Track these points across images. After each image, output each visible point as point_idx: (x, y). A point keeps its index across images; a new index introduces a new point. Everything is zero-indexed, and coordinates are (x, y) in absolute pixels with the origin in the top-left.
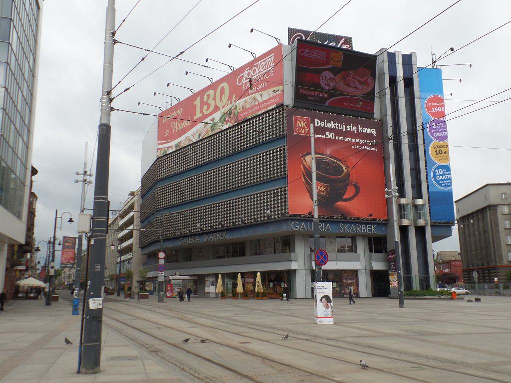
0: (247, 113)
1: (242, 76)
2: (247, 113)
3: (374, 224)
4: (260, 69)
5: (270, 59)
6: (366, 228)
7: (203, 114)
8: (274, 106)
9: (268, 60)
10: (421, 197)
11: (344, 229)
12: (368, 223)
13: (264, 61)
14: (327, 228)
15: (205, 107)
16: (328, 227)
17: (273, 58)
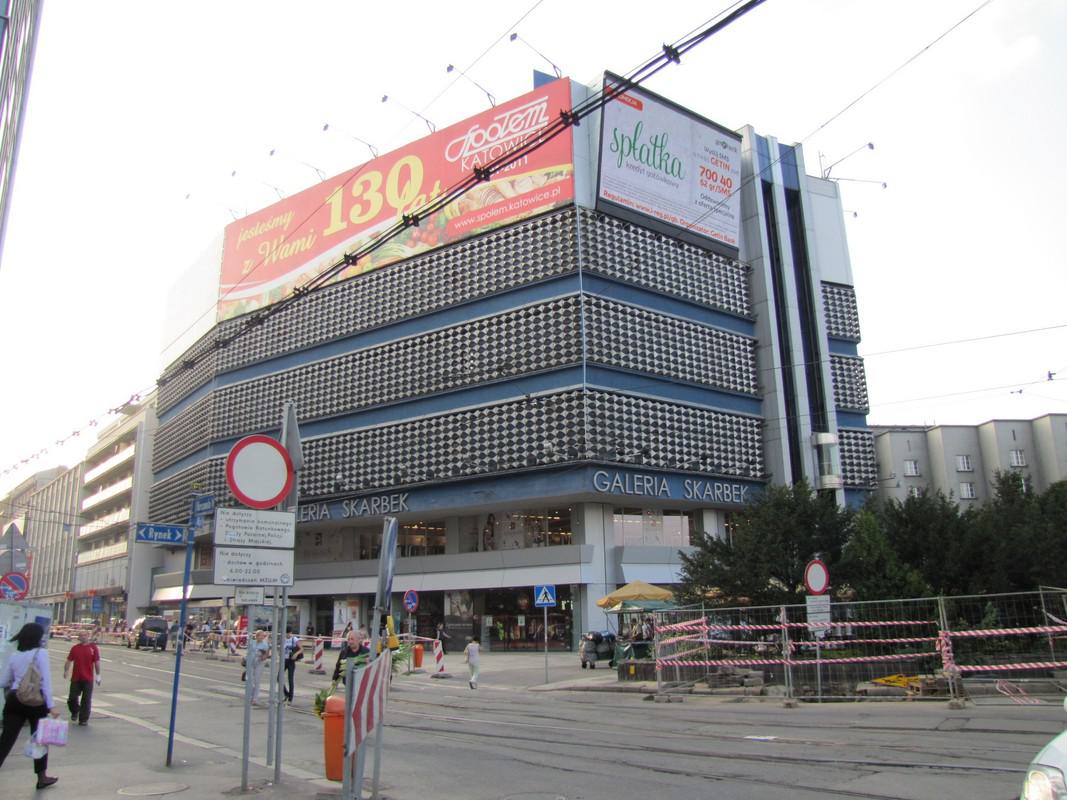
0: (472, 221)
1: (462, 142)
2: (472, 221)
4: (511, 129)
5: (538, 108)
7: (349, 222)
8: (550, 207)
9: (531, 111)
10: (825, 429)
13: (522, 112)
15: (357, 209)
16: (617, 482)
17: (545, 105)
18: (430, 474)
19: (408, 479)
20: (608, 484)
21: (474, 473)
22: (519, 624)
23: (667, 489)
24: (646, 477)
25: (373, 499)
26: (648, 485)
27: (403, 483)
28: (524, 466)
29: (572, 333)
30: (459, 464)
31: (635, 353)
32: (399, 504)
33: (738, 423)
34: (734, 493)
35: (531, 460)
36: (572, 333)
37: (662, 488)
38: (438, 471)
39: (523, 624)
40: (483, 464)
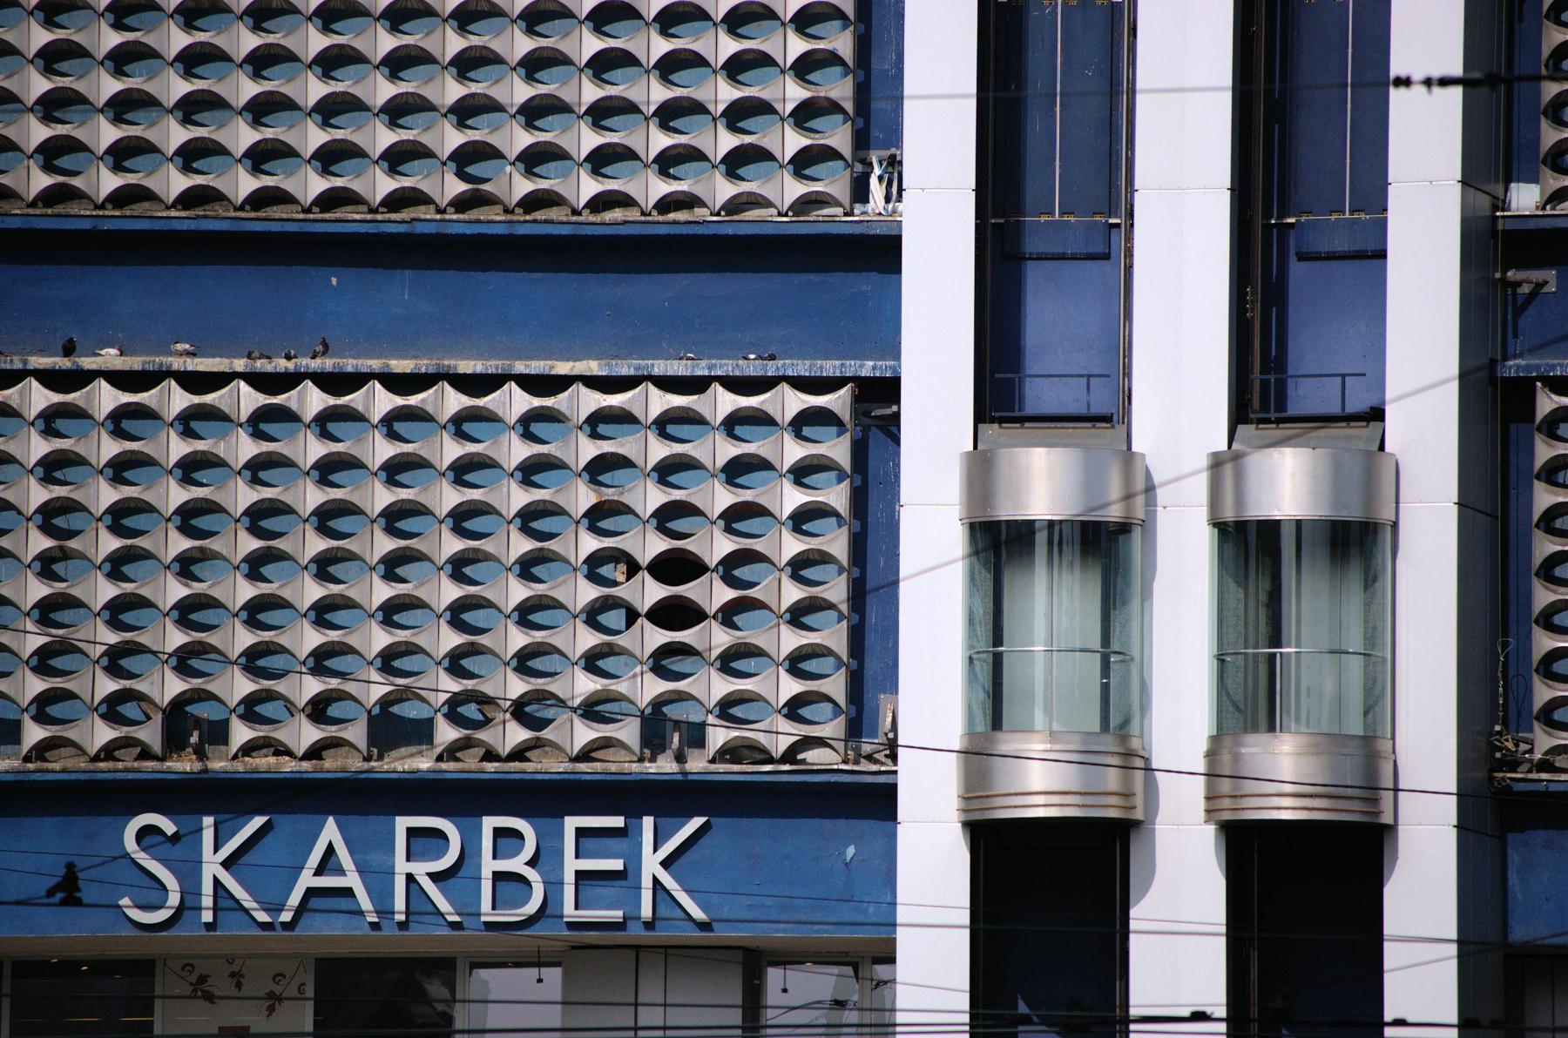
11: (189, 873)
16: (328, 863)
34: (572, 865)
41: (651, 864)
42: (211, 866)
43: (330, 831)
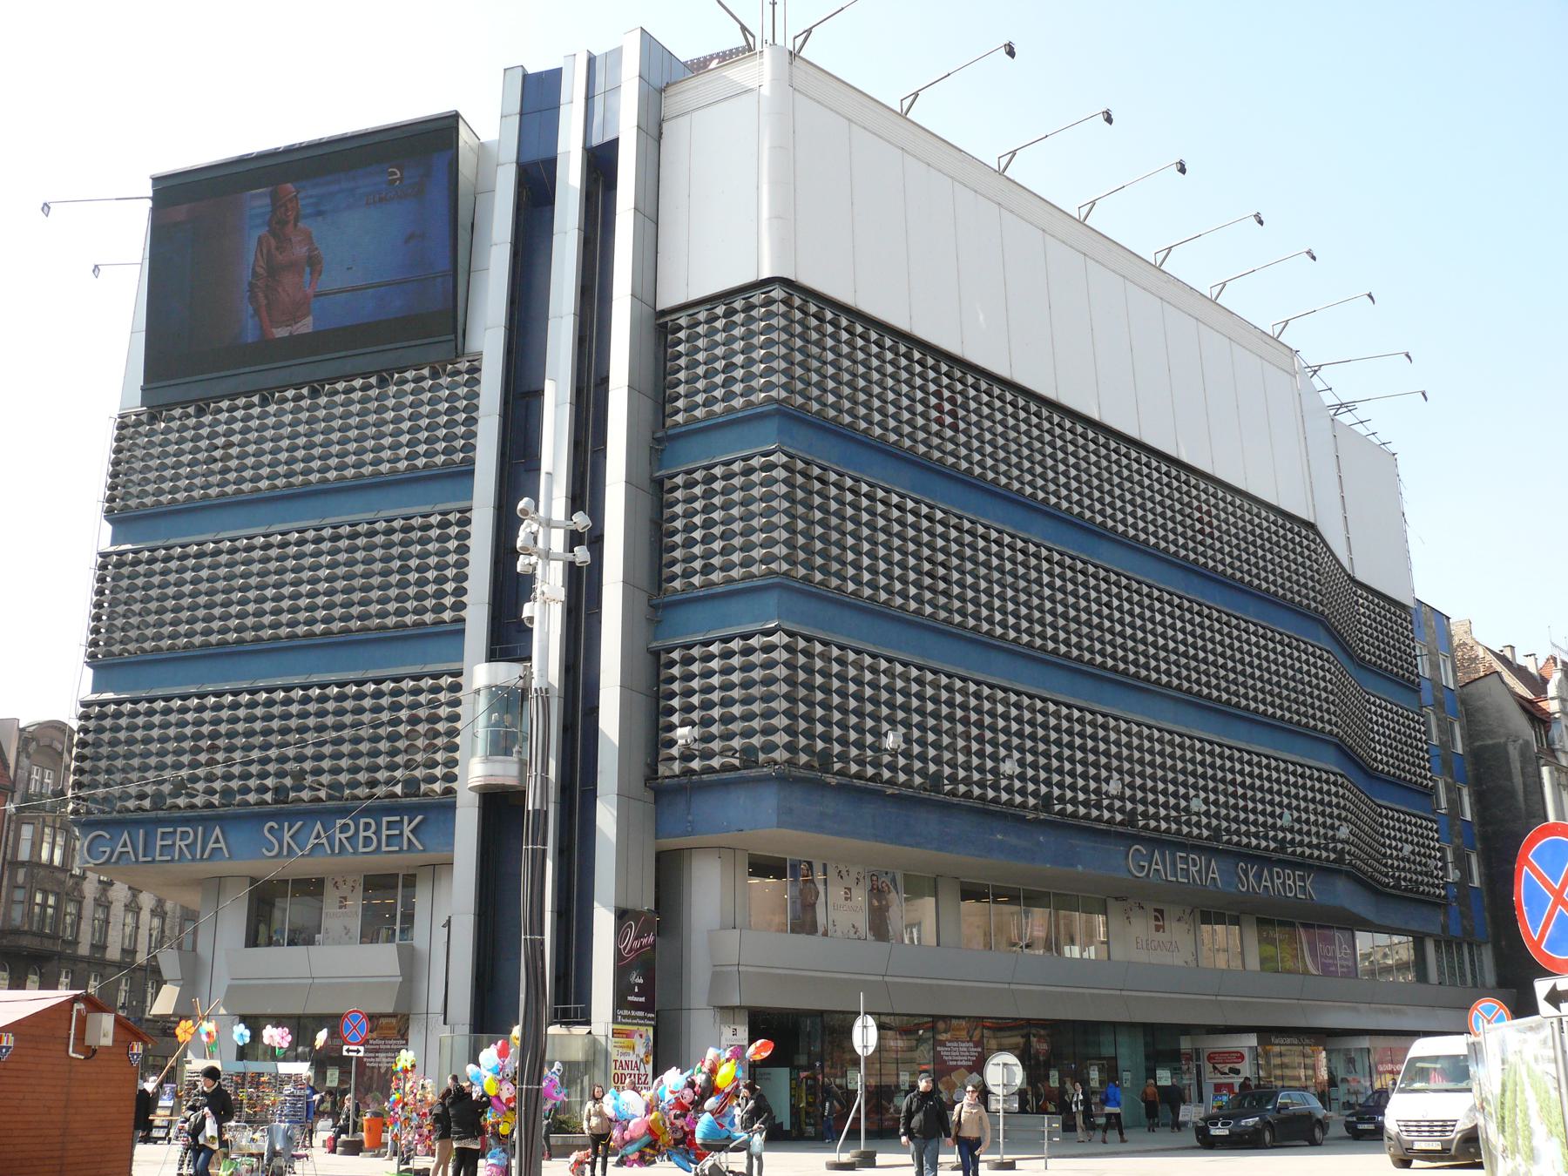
3: (411, 810)
6: (377, 832)
12: (389, 811)
14: (211, 845)
16: (217, 841)
18: (227, 793)
19: (305, 795)
20: (1146, 864)
21: (193, 807)
22: (328, 1084)
23: (1216, 876)
24: (179, 829)
25: (339, 822)
26: (1195, 869)
27: (171, 808)
28: (267, 803)
29: (449, 587)
30: (166, 788)
31: (873, 570)
32: (401, 834)
33: (1081, 721)
34: (385, 832)
35: (411, 785)
36: (449, 587)
37: (1211, 875)
38: (245, 790)
39: (335, 1084)
40: (210, 792)
41: (407, 831)
42: (287, 837)
43: (217, 830)
